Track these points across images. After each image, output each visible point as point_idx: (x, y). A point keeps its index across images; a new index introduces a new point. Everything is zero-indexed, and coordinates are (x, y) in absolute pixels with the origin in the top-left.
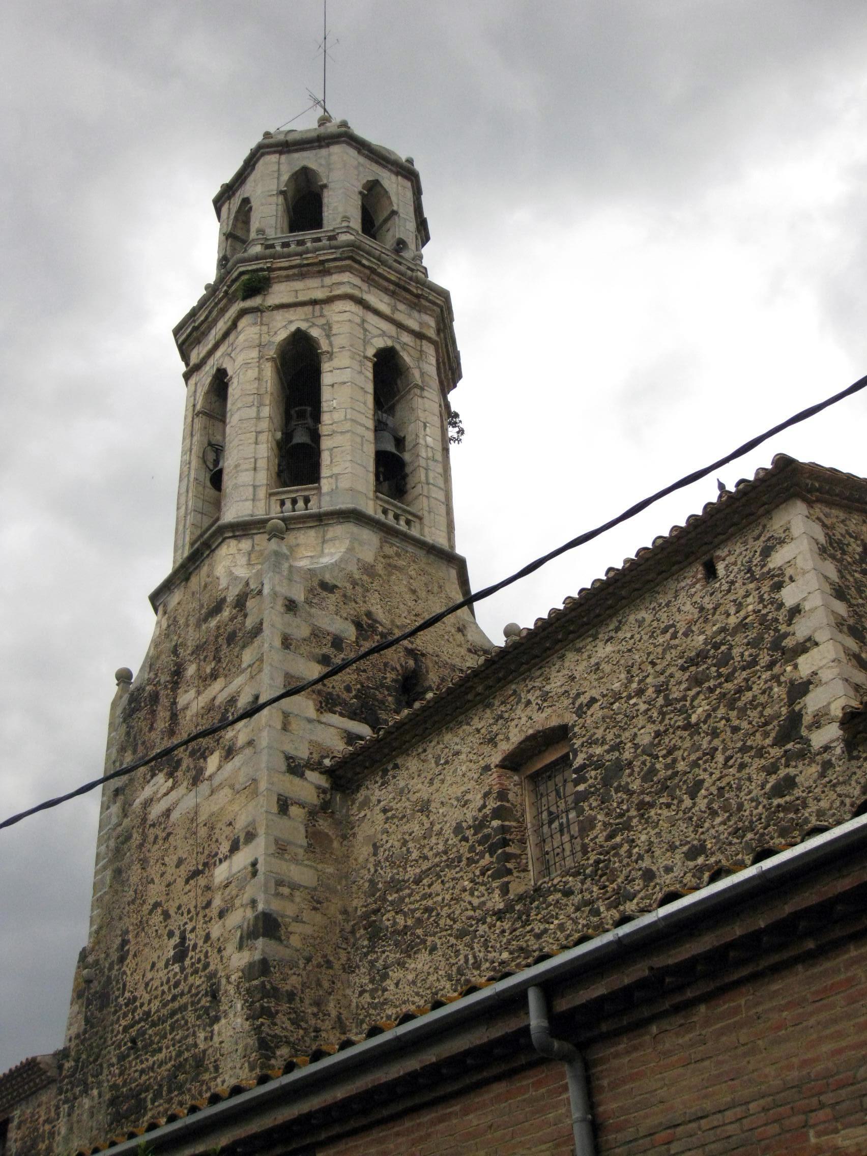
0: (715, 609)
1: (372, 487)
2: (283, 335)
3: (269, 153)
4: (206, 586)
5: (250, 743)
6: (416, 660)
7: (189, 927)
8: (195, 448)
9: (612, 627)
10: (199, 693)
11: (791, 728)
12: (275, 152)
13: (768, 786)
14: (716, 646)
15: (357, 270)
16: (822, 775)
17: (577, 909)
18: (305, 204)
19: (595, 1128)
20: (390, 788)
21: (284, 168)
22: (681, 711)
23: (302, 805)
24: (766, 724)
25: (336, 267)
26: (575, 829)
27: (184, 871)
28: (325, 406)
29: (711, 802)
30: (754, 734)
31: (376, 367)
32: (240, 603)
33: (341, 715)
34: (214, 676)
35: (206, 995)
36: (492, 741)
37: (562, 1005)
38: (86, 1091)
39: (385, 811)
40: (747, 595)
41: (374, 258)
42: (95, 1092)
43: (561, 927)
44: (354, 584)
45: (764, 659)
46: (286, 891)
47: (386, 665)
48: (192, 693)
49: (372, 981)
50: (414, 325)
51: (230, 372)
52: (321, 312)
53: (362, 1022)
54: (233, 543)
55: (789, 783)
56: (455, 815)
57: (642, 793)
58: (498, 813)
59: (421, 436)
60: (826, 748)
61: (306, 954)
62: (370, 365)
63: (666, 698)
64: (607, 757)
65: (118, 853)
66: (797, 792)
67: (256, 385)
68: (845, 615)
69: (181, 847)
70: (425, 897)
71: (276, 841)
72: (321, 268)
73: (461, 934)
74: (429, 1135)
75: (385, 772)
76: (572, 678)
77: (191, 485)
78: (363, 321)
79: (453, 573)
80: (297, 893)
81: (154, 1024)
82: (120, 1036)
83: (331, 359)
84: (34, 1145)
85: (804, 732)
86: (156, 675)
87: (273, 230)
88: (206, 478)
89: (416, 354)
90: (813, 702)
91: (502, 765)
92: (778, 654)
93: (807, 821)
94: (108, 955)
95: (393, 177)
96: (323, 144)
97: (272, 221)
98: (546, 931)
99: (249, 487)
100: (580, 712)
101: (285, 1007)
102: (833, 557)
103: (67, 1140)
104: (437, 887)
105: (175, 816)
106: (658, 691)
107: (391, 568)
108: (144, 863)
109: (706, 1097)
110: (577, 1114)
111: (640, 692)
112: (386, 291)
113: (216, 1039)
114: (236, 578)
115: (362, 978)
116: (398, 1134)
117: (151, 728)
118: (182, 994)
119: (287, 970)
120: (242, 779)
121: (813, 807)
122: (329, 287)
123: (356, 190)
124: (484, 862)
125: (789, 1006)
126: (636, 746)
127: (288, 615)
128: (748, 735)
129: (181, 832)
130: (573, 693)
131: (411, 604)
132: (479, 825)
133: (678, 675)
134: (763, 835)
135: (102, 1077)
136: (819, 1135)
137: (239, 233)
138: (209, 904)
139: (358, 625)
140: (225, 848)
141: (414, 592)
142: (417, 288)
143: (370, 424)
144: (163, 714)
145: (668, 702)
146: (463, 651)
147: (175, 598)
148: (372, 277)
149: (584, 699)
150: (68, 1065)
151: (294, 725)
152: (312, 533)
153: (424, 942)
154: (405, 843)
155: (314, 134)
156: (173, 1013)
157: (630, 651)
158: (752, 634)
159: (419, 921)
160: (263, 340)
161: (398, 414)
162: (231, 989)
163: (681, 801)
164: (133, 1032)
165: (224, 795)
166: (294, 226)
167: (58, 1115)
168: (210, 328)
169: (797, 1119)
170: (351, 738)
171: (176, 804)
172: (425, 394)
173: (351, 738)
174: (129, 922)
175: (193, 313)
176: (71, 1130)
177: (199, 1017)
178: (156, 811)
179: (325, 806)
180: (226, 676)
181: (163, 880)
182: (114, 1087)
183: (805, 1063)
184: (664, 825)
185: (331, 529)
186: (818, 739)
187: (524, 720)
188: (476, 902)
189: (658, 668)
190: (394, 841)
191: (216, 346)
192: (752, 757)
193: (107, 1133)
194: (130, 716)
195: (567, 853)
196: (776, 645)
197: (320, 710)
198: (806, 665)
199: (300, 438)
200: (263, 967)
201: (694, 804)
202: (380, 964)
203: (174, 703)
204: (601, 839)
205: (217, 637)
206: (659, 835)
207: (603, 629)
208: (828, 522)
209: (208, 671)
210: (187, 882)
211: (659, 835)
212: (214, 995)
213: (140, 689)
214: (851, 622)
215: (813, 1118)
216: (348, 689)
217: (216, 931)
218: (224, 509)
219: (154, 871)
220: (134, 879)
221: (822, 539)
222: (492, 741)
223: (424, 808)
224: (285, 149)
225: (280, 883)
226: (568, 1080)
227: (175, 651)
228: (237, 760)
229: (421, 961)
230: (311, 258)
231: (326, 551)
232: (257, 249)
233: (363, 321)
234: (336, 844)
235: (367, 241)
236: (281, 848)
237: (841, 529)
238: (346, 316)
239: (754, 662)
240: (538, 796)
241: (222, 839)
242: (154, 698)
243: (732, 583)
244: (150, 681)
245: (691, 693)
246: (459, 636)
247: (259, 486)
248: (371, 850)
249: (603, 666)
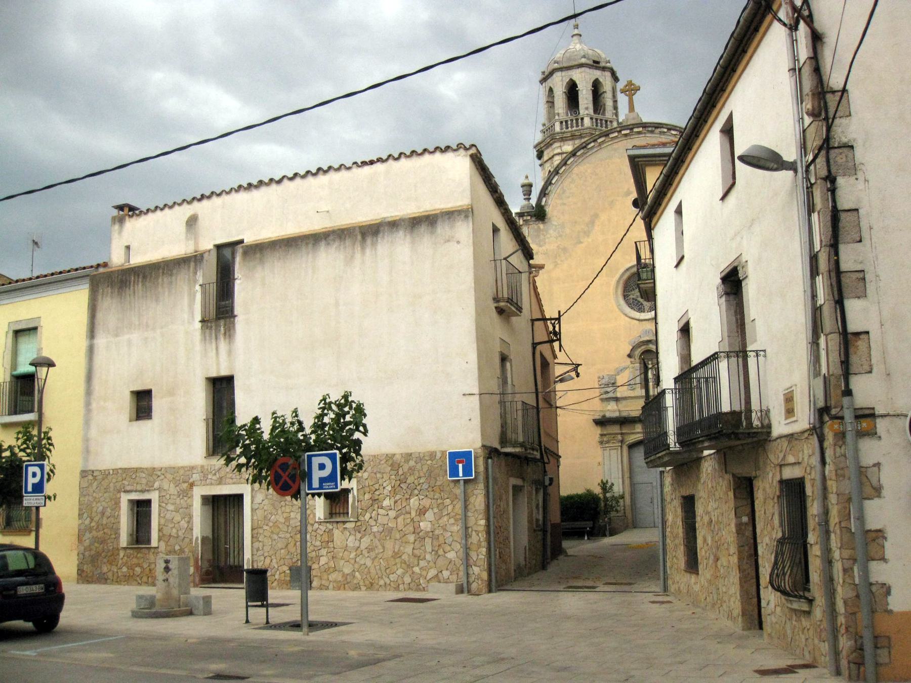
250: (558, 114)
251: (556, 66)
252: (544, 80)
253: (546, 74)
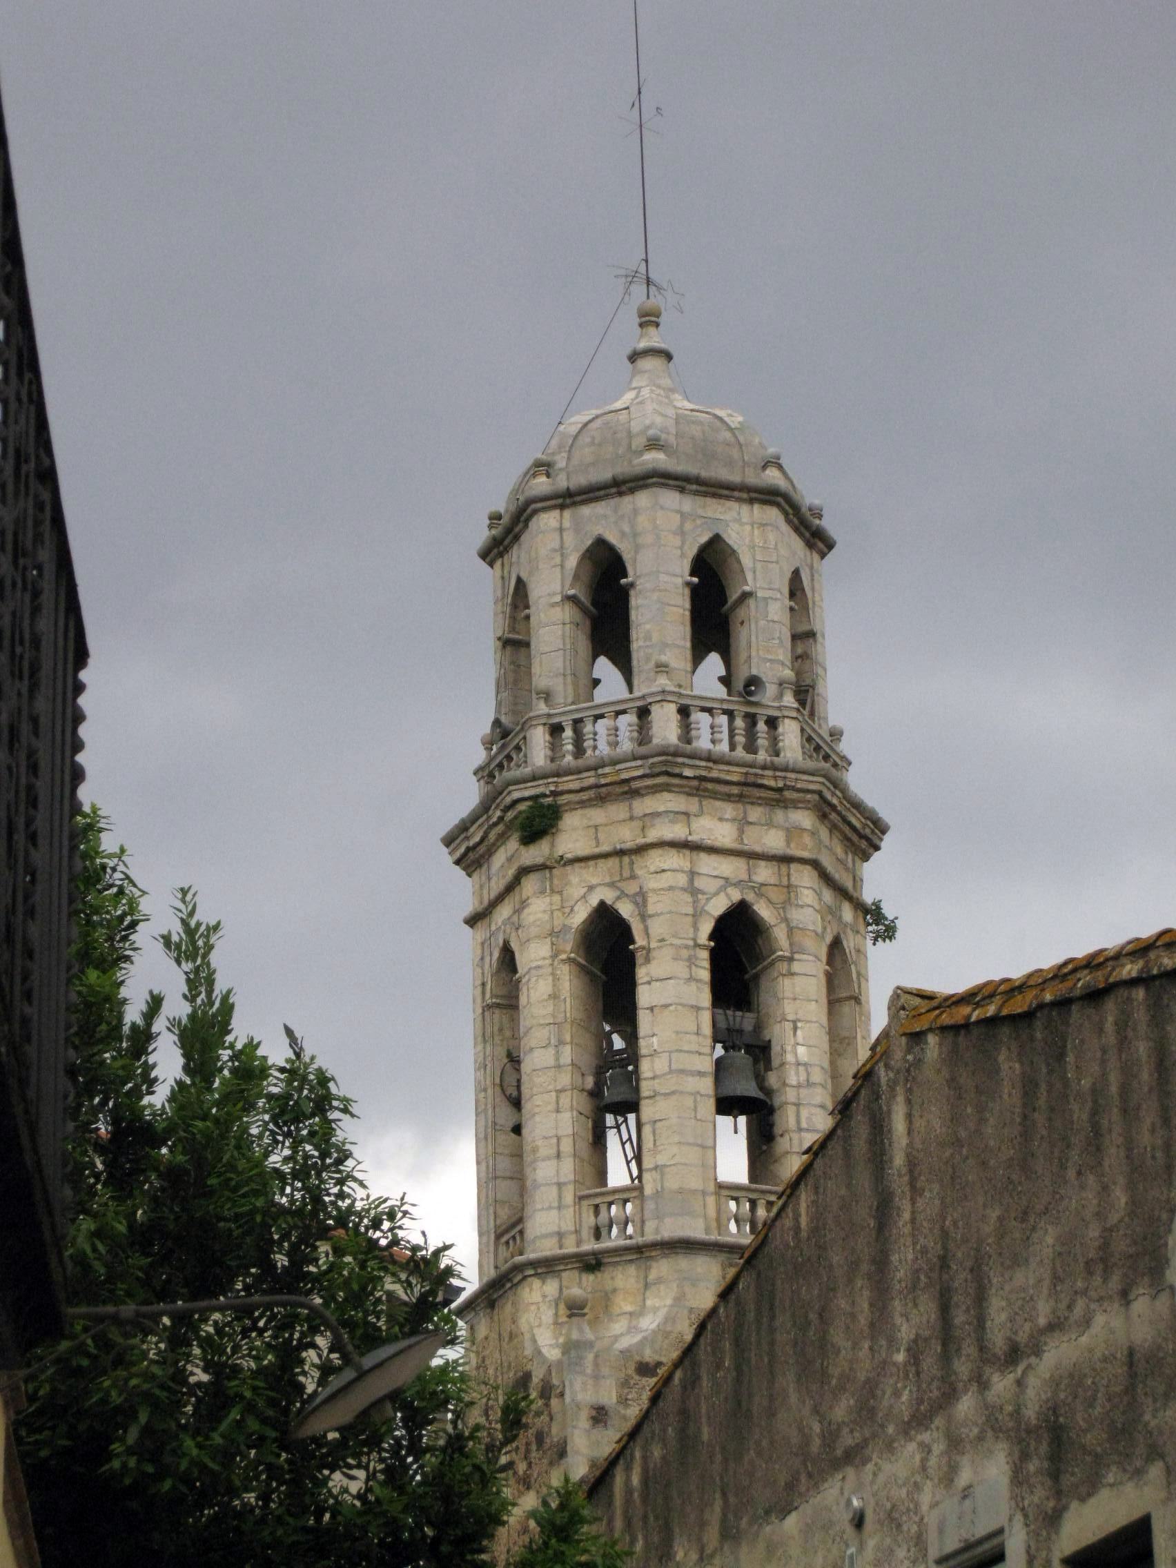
2: (581, 915)
12: (554, 507)
15: (677, 786)
25: (647, 787)
41: (701, 759)
52: (632, 870)
54: (536, 1283)
59: (789, 1048)
62: (705, 955)
67: (550, 1009)
72: (626, 789)
83: (648, 960)
87: (561, 679)
95: (745, 509)
96: (624, 488)
112: (728, 798)
122: (640, 818)
123: (679, 581)
127: (595, 1431)
142: (775, 778)
152: (632, 1270)
160: (556, 923)
172: (796, 967)
185: (654, 1264)
224: (568, 501)
231: (649, 1303)
233: (692, 874)
238: (666, 880)
247: (565, 1184)
250: (547, 696)
251: (541, 485)
252: (494, 551)
253: (506, 520)
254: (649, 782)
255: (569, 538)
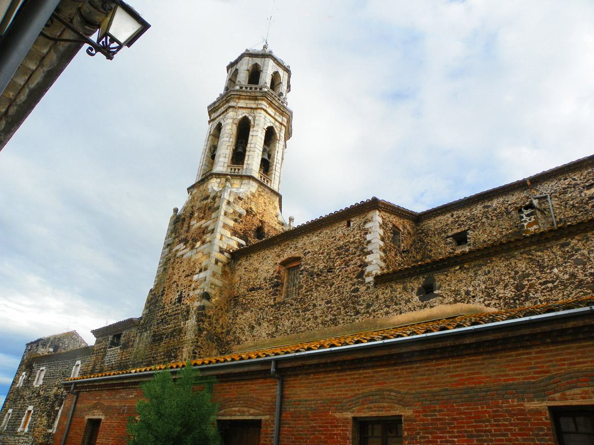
0: (348, 235)
1: (258, 170)
2: (240, 117)
3: (247, 56)
4: (204, 190)
5: (210, 241)
6: (262, 224)
7: (184, 291)
8: (208, 146)
9: (318, 232)
10: (197, 222)
11: (361, 275)
13: (352, 289)
14: (346, 246)
16: (366, 290)
17: (293, 310)
18: (255, 75)
19: (282, 397)
20: (248, 262)
21: (250, 62)
22: (333, 262)
23: (222, 262)
24: (354, 272)
26: (297, 287)
27: (184, 274)
28: (249, 142)
29: (335, 289)
30: (351, 273)
31: (267, 132)
32: (214, 198)
33: (238, 237)
34: (203, 218)
35: (185, 312)
36: (279, 256)
37: (280, 366)
38: (146, 331)
39: (245, 268)
40: (357, 234)
42: (149, 332)
43: (288, 314)
44: (248, 198)
45: (358, 253)
46: (213, 287)
47: (253, 224)
48: (195, 222)
49: (233, 316)
50: (280, 121)
51: (223, 125)
53: (228, 327)
54: (215, 179)
55: (357, 290)
56: (265, 275)
57: (318, 282)
58: (276, 277)
60: (369, 283)
61: (216, 305)
62: (265, 131)
63: (329, 257)
64: (310, 269)
65: (166, 263)
66: (359, 293)
68: (383, 246)
69: (185, 266)
70: (252, 296)
71: (213, 272)
73: (260, 309)
74: (242, 387)
75: (247, 257)
76: (305, 244)
77: (205, 157)
78: (265, 117)
79: (278, 199)
80: (216, 288)
81: (169, 316)
82: (159, 317)
83: (253, 127)
84: (128, 343)
85: (364, 277)
86: (186, 213)
88: (210, 155)
89: (279, 129)
90: (368, 269)
91: (280, 264)
92: (362, 253)
93: (360, 301)
94: (158, 293)
97: (244, 79)
98: (284, 314)
99: (222, 164)
100: (305, 254)
101: (207, 320)
102: (383, 228)
103: (138, 344)
104: (256, 294)
105: (184, 257)
106: (327, 255)
107: (260, 195)
108: (173, 269)
109: (309, 396)
110: (278, 393)
111: (322, 253)
112: (274, 108)
113: (186, 325)
114: (214, 190)
115: (230, 314)
116: (234, 385)
117: (181, 229)
118: (179, 310)
119: (210, 310)
120: (206, 251)
121: (362, 298)
124: (270, 290)
125: (332, 381)
126: (318, 268)
128: (349, 273)
129: (185, 262)
130: (304, 248)
131: (264, 206)
132: (271, 280)
133: (334, 251)
134: (347, 302)
135: (151, 328)
136: (331, 412)
137: (233, 79)
138: (190, 286)
139: (247, 211)
140: (198, 270)
141: (265, 203)
143: (262, 150)
144: (186, 225)
145: (329, 258)
146: (276, 223)
147: (195, 191)
148: (271, 104)
149: (307, 251)
150: (142, 322)
151: (224, 239)
152: (239, 180)
153: (250, 309)
154: (249, 279)
155: (261, 53)
156: (175, 315)
157: (322, 241)
158: (356, 245)
159: (249, 303)
161: (271, 147)
162: (193, 312)
163: (327, 287)
164: (163, 317)
165: (200, 255)
166: (250, 82)
167: (137, 336)
168: (219, 109)
169: (328, 408)
170: (239, 245)
171: (185, 253)
173: (239, 245)
174: (166, 285)
175: (214, 103)
176: (140, 341)
177: (182, 317)
178: (179, 254)
179: (228, 263)
180: (206, 219)
181: (178, 275)
182: (155, 331)
183: (332, 395)
184: (321, 293)
186: (368, 279)
187: (289, 253)
188: (266, 301)
189: (329, 248)
190: (246, 278)
191: (220, 115)
192: (349, 280)
193: (150, 344)
194: (176, 222)
195: (294, 293)
196: (362, 250)
197: (232, 235)
198: (369, 258)
199: (240, 150)
200: (202, 308)
201: (331, 289)
202: (236, 312)
203: (190, 223)
204: (303, 292)
205: (206, 206)
206: (320, 295)
207: (316, 232)
208: (384, 217)
209: (201, 216)
210: (185, 277)
211: (320, 295)
212: (188, 312)
213: (180, 216)
214: (384, 248)
215: (332, 408)
216: (241, 230)
217: (191, 294)
218: (214, 167)
219: (176, 271)
220: (169, 272)
221: (381, 223)
222: (279, 256)
223: (256, 270)
225: (212, 284)
226: (278, 383)
227: (192, 207)
228: (205, 246)
229: (248, 314)
230: (253, 94)
232: (238, 88)
233: (265, 117)
234: (230, 275)
235: (271, 91)
236: (214, 274)
237: (388, 219)
239: (355, 253)
240: (289, 274)
241: (197, 268)
242: (184, 220)
243: (354, 229)
244: (183, 214)
245: (336, 257)
246: (276, 218)
248: (239, 279)
249: (314, 243)
254: (261, 98)
255: (250, 62)
